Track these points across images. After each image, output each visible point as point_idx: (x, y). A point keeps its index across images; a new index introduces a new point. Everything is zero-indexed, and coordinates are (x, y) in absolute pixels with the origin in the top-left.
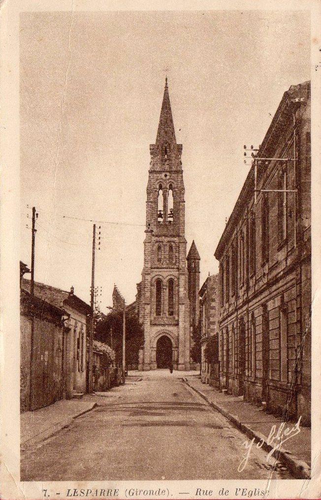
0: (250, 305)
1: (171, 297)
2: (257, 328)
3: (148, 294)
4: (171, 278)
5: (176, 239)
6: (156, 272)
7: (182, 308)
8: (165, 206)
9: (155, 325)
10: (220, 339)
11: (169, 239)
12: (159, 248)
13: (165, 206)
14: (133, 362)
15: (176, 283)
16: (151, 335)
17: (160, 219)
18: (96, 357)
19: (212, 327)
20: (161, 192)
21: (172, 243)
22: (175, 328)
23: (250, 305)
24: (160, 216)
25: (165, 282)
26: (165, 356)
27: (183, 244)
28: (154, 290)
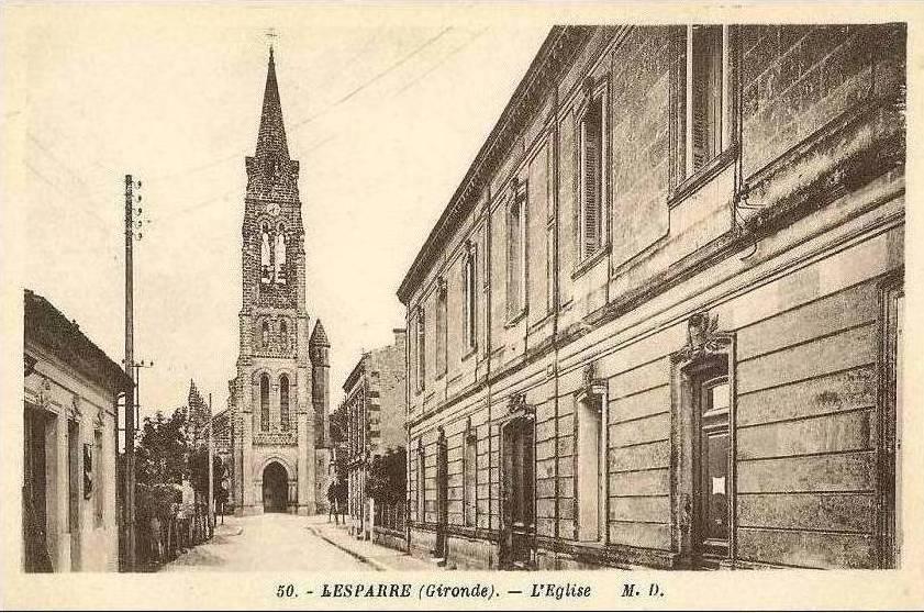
0: (561, 356)
1: (285, 404)
2: (497, 433)
3: (248, 397)
4: (284, 374)
5: (290, 312)
6: (261, 363)
7: (302, 419)
8: (272, 259)
9: (261, 444)
10: (413, 464)
11: (282, 311)
12: (265, 326)
13: (272, 259)
14: (228, 504)
15: (291, 380)
16: (255, 459)
17: (264, 280)
18: (808, 438)
19: (374, 441)
20: (266, 237)
21: (286, 319)
22: (293, 450)
23: (561, 356)
24: (266, 274)
25: (274, 380)
26: (279, 492)
27: (303, 320)
28: (258, 389)
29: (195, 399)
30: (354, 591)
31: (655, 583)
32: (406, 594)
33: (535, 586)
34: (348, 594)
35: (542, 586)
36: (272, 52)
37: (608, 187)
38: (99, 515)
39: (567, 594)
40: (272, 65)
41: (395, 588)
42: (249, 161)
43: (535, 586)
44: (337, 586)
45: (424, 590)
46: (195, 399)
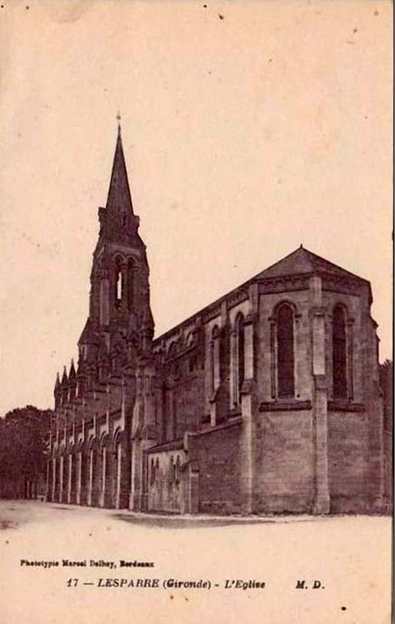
29: (387, 361)
30: (119, 582)
31: (140, 578)
32: (155, 585)
33: (228, 582)
34: (116, 585)
35: (234, 582)
36: (119, 128)
37: (64, 468)
38: (153, 462)
39: (142, 581)
40: (119, 138)
41: (148, 582)
42: (101, 209)
43: (228, 582)
44: (108, 580)
45: (166, 583)
46: (387, 361)
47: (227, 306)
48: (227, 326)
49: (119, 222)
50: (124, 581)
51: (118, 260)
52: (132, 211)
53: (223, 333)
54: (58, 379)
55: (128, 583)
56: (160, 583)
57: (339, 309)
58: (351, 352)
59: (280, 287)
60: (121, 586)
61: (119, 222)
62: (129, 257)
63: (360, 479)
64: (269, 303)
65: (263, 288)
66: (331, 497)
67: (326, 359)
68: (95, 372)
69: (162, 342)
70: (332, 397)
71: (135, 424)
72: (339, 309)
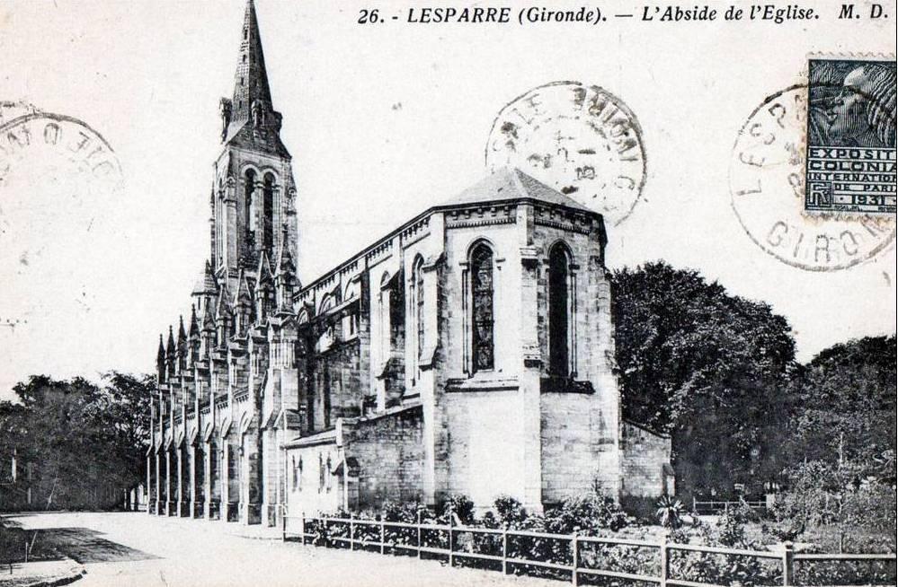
30: (444, 15)
45: (525, 14)
47: (401, 244)
48: (401, 274)
49: (256, 115)
50: (451, 12)
51: (250, 173)
52: (272, 107)
53: (395, 285)
54: (161, 346)
55: (458, 15)
56: (513, 15)
57: (559, 253)
58: (574, 309)
59: (475, 219)
60: (446, 20)
61: (256, 115)
62: (265, 171)
63: (587, 482)
64: (461, 242)
65: (450, 220)
66: (547, 507)
67: (540, 319)
68: (213, 334)
69: (311, 292)
70: (547, 372)
71: (268, 409)
72: (559, 253)
